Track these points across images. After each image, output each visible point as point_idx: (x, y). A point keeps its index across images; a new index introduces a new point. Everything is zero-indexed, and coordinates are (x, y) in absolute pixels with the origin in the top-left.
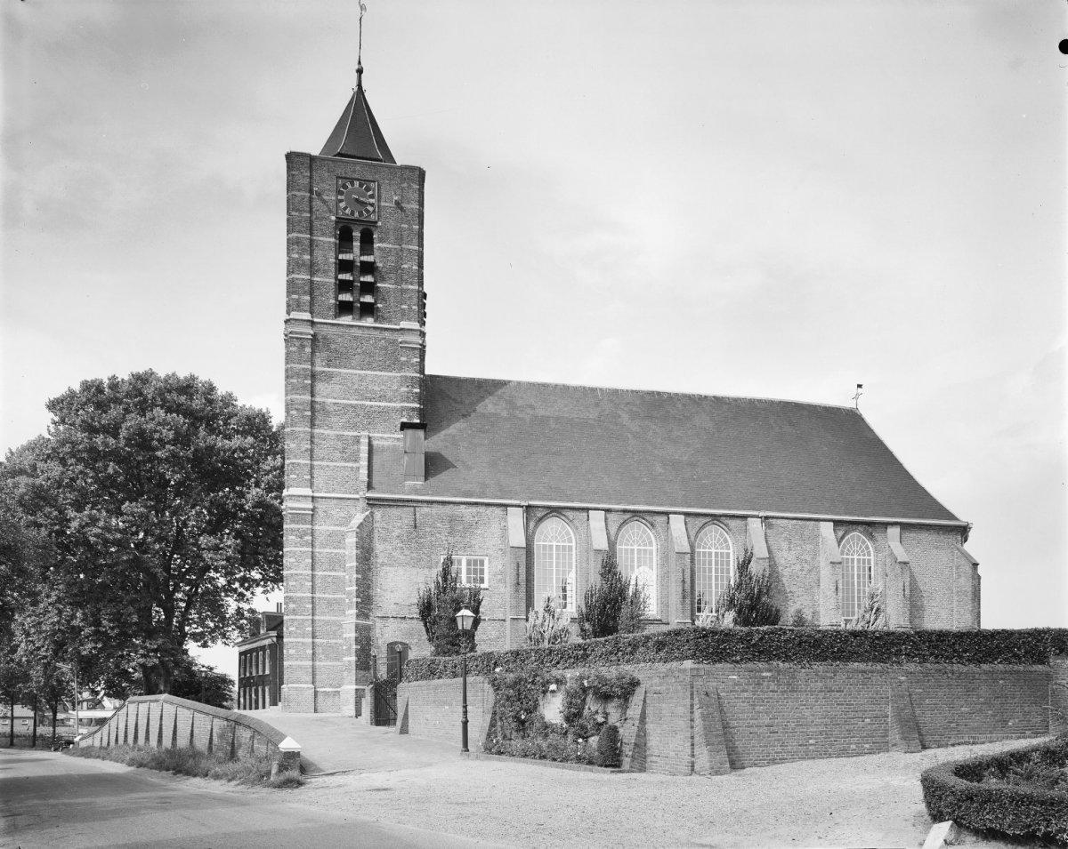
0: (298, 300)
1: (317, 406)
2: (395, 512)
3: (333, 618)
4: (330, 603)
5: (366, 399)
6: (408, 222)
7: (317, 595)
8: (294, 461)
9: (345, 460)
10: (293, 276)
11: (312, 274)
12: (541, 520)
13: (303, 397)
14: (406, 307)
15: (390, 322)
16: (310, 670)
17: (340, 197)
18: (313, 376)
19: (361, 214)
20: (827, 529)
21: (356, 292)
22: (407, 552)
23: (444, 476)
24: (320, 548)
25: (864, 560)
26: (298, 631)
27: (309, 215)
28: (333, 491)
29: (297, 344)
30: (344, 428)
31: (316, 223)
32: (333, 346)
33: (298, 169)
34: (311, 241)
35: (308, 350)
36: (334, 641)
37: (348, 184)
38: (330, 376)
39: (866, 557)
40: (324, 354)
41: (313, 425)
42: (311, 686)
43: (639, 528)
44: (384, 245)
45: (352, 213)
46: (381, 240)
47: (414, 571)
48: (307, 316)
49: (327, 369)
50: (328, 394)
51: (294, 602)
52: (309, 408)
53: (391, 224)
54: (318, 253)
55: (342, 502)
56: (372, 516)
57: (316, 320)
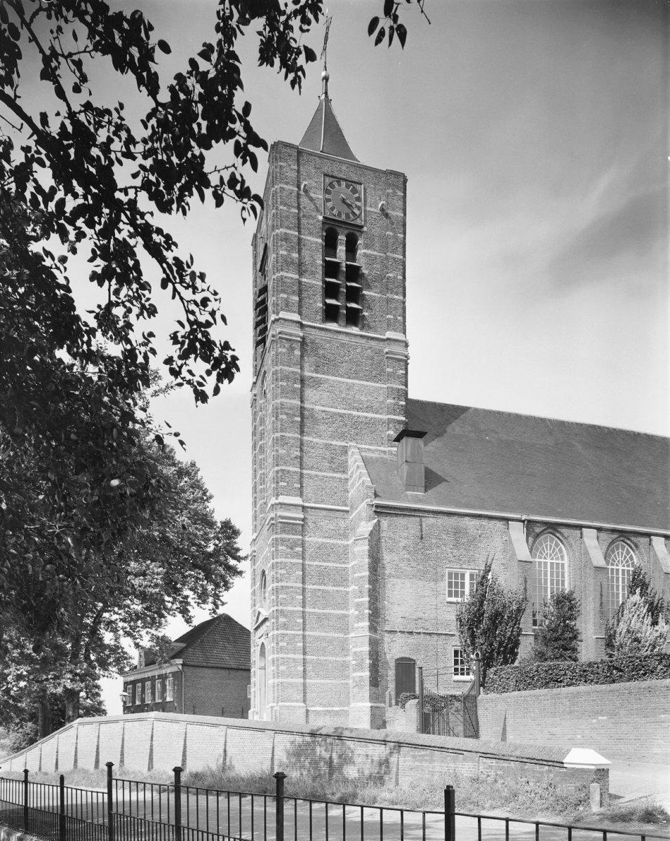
0: (286, 300)
1: (306, 413)
2: (402, 521)
3: (324, 634)
4: (319, 617)
5: (354, 408)
6: (393, 230)
7: (308, 609)
8: (284, 468)
9: (334, 471)
10: (282, 273)
11: (301, 274)
12: (538, 535)
13: (292, 401)
14: (392, 317)
15: (376, 331)
16: (302, 688)
17: (327, 196)
18: (302, 381)
19: (347, 215)
20: (517, 533)
21: (342, 298)
22: (414, 564)
23: (440, 488)
24: (310, 560)
25: (558, 564)
26: (289, 647)
27: (297, 211)
28: (322, 502)
29: (287, 345)
30: (332, 437)
31: (304, 221)
32: (321, 352)
33: (286, 161)
34: (300, 239)
35: (297, 353)
36: (323, 658)
37: (335, 184)
38: (317, 383)
39: (560, 562)
40: (312, 359)
41: (302, 432)
42: (303, 704)
43: (552, 541)
44: (369, 252)
45: (340, 214)
46: (367, 247)
47: (421, 583)
48: (296, 317)
49: (315, 375)
50: (316, 401)
51: (285, 616)
52: (298, 413)
53: (376, 231)
54: (305, 252)
55: (331, 514)
56: (379, 524)
57: (304, 322)
